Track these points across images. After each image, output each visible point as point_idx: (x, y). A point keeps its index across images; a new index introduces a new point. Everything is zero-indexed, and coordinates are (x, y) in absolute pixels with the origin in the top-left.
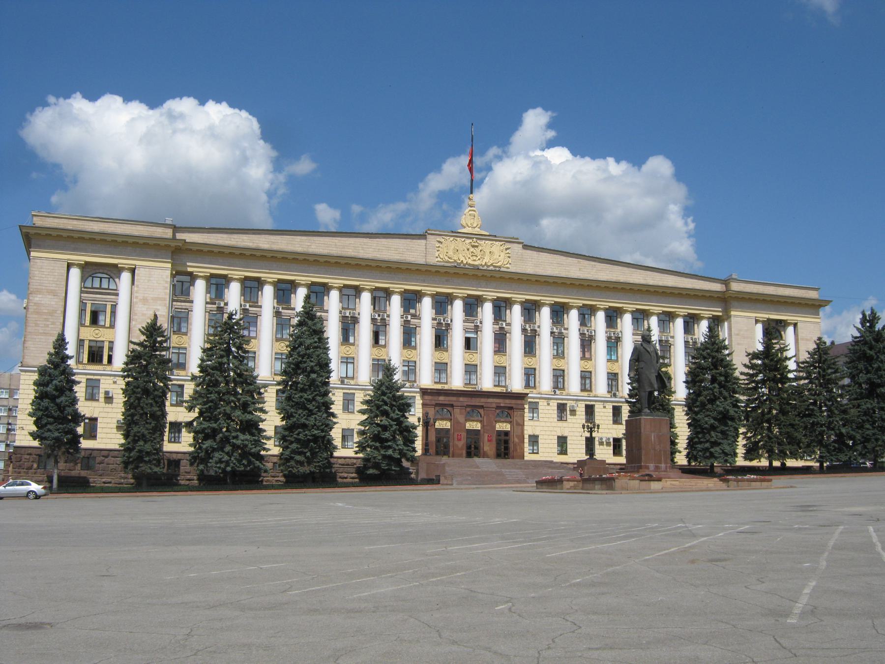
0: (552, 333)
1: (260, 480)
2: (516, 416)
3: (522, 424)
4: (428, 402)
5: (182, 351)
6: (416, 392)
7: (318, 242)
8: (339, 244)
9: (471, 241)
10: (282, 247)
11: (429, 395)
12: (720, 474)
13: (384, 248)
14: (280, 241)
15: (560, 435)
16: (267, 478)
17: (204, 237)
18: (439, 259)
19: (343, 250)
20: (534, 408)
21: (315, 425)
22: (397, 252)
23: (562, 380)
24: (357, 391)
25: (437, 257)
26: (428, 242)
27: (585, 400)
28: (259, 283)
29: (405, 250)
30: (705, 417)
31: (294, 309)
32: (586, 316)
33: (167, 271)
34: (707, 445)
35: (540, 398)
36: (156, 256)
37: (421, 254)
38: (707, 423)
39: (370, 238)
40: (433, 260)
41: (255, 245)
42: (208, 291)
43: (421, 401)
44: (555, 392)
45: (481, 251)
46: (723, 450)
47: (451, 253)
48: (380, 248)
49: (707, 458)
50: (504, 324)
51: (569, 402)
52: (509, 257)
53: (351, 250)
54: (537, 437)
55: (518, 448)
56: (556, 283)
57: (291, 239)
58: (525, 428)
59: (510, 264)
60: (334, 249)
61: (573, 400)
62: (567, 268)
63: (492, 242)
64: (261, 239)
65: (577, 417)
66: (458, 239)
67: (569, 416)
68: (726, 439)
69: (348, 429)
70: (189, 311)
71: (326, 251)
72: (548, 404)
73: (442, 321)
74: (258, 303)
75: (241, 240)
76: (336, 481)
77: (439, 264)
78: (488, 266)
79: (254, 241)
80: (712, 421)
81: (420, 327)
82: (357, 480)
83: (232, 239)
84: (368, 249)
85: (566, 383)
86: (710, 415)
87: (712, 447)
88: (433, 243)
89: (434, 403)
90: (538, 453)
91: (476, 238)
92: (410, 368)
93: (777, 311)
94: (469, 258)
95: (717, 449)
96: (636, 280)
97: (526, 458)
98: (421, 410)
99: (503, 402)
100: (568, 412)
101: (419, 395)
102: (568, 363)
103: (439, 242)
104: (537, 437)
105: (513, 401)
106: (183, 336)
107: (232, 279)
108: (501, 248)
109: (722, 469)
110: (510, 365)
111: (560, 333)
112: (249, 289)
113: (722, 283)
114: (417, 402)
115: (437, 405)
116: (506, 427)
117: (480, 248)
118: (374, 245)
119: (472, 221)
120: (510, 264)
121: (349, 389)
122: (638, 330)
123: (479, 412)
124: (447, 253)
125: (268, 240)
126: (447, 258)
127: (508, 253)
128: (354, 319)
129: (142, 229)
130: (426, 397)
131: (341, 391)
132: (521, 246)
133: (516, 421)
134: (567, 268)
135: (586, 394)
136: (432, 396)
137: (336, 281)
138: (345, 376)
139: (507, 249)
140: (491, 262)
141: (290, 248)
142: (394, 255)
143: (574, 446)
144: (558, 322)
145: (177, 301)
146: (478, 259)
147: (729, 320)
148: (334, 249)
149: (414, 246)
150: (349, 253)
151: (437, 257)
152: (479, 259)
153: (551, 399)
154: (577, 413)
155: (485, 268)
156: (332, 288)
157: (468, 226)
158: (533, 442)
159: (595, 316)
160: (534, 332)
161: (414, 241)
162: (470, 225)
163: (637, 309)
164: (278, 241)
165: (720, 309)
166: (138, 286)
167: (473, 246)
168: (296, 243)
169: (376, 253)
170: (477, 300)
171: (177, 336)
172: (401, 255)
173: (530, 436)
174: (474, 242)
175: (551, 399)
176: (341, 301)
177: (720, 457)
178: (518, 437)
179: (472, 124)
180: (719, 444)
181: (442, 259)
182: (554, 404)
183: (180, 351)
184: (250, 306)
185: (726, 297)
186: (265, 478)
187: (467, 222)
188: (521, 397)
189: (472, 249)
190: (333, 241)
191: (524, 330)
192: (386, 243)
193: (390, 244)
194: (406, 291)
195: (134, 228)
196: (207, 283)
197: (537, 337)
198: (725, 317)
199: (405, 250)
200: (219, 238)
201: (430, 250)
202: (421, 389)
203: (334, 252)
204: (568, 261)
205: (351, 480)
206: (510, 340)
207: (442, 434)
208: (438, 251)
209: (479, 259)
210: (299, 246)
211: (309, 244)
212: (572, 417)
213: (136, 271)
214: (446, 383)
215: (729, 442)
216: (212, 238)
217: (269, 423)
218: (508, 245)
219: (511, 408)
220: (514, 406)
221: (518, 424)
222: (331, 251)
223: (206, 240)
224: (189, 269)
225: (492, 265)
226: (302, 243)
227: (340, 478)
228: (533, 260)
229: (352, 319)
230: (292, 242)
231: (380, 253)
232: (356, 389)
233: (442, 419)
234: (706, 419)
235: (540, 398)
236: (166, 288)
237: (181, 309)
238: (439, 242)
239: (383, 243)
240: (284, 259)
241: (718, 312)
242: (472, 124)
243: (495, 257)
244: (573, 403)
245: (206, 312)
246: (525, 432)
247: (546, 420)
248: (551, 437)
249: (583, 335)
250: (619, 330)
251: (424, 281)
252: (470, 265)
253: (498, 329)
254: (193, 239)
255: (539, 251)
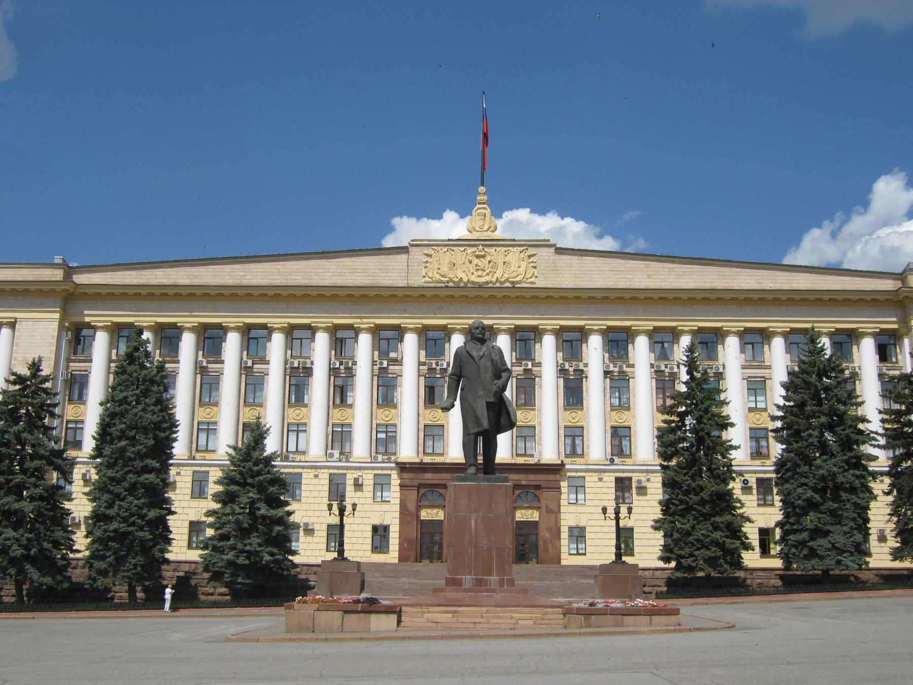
0: (607, 373)
1: (109, 596)
2: (546, 499)
3: (556, 510)
4: (408, 482)
5: (77, 425)
6: (391, 469)
7: (256, 270)
8: (284, 270)
9: (474, 249)
10: (206, 281)
11: (408, 472)
12: (873, 584)
13: (347, 271)
14: (204, 274)
15: (377, 522)
16: (121, 594)
17: (107, 277)
18: (427, 279)
19: (290, 277)
20: (578, 487)
21: (118, 515)
22: (366, 274)
23: (628, 443)
24: (305, 470)
25: (424, 277)
26: (411, 257)
27: (373, 468)
28: (628, 335)
29: (377, 271)
30: (799, 487)
31: (900, 368)
32: (666, 345)
33: (55, 323)
34: (805, 535)
35: (586, 471)
36: (41, 306)
37: (401, 275)
38: (800, 498)
39: (327, 258)
40: (417, 280)
41: (172, 280)
42: (652, 349)
43: (399, 481)
44: (612, 461)
45: (489, 262)
46: (833, 544)
47: (445, 269)
48: (341, 271)
49: (806, 557)
50: (530, 364)
51: (635, 474)
52: (535, 268)
53: (300, 278)
54: (582, 529)
55: (550, 546)
56: (622, 298)
57: (218, 270)
58: (563, 516)
59: (536, 277)
60: (278, 277)
61: (642, 471)
62: (627, 276)
63: (506, 249)
64: (180, 273)
65: (648, 497)
66: (455, 248)
67: (635, 497)
68: (840, 523)
69: (577, 527)
70: (398, 376)
71: (266, 281)
72: (601, 480)
73: (434, 366)
74: (764, 361)
75: (153, 277)
76: (199, 598)
77: (426, 285)
78: (502, 283)
79: (171, 277)
80: (810, 493)
81: (634, 378)
82: (228, 598)
83: (143, 277)
84: (324, 274)
85: (633, 447)
86: (805, 484)
87: (812, 539)
88: (419, 257)
89: (416, 483)
90: (585, 554)
91: (483, 245)
92: (389, 434)
93: (435, 314)
94: (473, 274)
95: (821, 541)
96: (743, 285)
97: (563, 563)
98: (398, 495)
99: (524, 479)
100: (634, 491)
101: (395, 472)
102: (634, 417)
103: (428, 255)
104: (582, 529)
105: (542, 477)
106: (81, 406)
107: (545, 331)
108: (522, 255)
109: (877, 575)
110: (540, 424)
111: (621, 372)
112: (750, 346)
113: (895, 279)
114: (393, 482)
115: (420, 486)
116: (533, 515)
117: (488, 258)
118: (333, 267)
119: (481, 222)
120: (536, 277)
121: (293, 467)
122: (754, 360)
123: (536, 495)
124: (439, 269)
125: (188, 274)
126: (438, 277)
127: (532, 262)
128: (308, 370)
129: (27, 273)
130: (406, 475)
131: (371, 471)
132: (552, 250)
133: (547, 506)
134: (627, 276)
135: (758, 462)
136: (413, 472)
137: (276, 320)
138: (295, 450)
139: (530, 256)
140: (506, 276)
141: (217, 281)
142: (361, 278)
143: (354, 540)
144: (619, 357)
145: (75, 361)
146: (485, 274)
147: (909, 334)
148: (278, 277)
149: (391, 264)
150: (297, 281)
151: (424, 277)
152: (488, 274)
153: (605, 471)
154: (649, 491)
155: (498, 285)
156: (545, 331)
157: (475, 230)
158: (577, 537)
159: (587, 342)
160: (579, 373)
161: (391, 256)
162: (478, 229)
163: (882, 330)
164: (202, 274)
165: (895, 319)
166: (17, 344)
167: (478, 257)
168: (226, 274)
169: (336, 278)
170: (849, 336)
171: (72, 406)
172: (372, 278)
173: (571, 529)
174: (480, 251)
175: (605, 471)
176: (742, 351)
177: (829, 555)
178: (550, 530)
179: (484, 93)
180: (826, 534)
181: (431, 278)
182: (610, 480)
183: (78, 426)
184: (208, 362)
185: (901, 299)
186: (117, 594)
187: (474, 225)
188: (556, 469)
189: (475, 261)
190: (276, 267)
191: (562, 372)
192: (350, 264)
193: (356, 264)
194: (610, 329)
195: (17, 273)
196: (512, 339)
197: (584, 380)
198: (903, 331)
199: (377, 271)
200: (126, 277)
201: (413, 268)
202: (397, 463)
203: (277, 281)
204: (629, 265)
205: (220, 597)
206: (540, 387)
207: (431, 529)
208: (426, 267)
209: (488, 274)
210: (229, 277)
211: (243, 274)
212: (641, 498)
213: (17, 326)
214: (442, 455)
215: (844, 528)
216: (117, 277)
217: (182, 517)
218: (532, 251)
219: (538, 487)
220: (543, 484)
221: (549, 511)
222: (272, 281)
223: (110, 280)
224: (87, 319)
225: (507, 280)
226: (234, 274)
227: (203, 594)
228: (573, 269)
229: (305, 371)
230: (220, 274)
231: (341, 278)
232: (303, 467)
233: (432, 507)
234: (800, 490)
235: (586, 471)
236: (51, 345)
237: (80, 371)
238: (428, 255)
239: (346, 264)
240: (206, 296)
241: (890, 323)
242: (484, 93)
243: (512, 268)
244: (642, 477)
245: (419, 376)
246: (563, 522)
247: (310, 500)
248: (362, 527)
249: (659, 374)
250: (856, 365)
251: (405, 311)
252: (473, 283)
253: (522, 373)
254: (94, 280)
255: (581, 255)
